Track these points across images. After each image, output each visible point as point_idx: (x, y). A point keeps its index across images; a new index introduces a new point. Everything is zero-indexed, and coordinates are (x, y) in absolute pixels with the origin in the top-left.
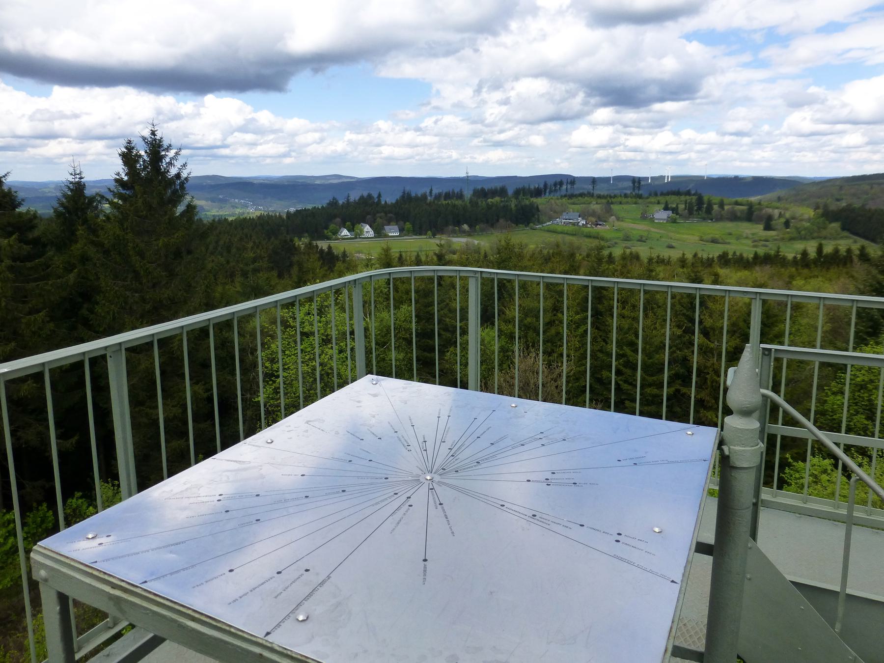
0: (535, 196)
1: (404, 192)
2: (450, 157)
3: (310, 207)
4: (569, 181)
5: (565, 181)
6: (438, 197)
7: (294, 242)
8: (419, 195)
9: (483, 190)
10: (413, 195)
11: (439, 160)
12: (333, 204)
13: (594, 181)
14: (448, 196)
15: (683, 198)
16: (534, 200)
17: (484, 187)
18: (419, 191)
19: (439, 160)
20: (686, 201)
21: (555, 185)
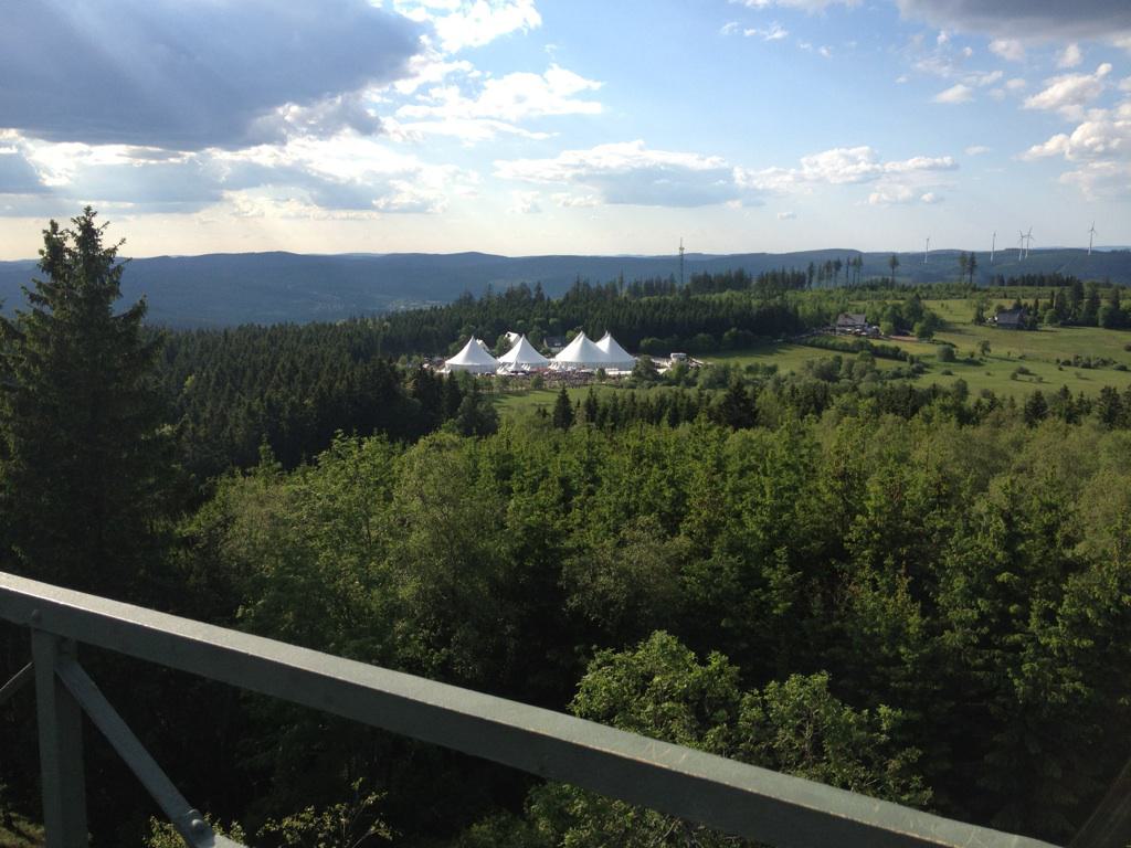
0: (792, 288)
1: (578, 283)
2: (28, 830)
3: (426, 307)
4: (851, 261)
5: (844, 263)
6: (635, 290)
7: (546, 298)
8: (603, 286)
9: (707, 277)
10: (593, 285)
11: (666, 181)
12: (467, 301)
13: (894, 260)
14: (651, 288)
15: (1047, 290)
16: (790, 295)
17: (527, 282)
18: (598, 280)
19: (666, 181)
20: (1053, 293)
21: (828, 266)
